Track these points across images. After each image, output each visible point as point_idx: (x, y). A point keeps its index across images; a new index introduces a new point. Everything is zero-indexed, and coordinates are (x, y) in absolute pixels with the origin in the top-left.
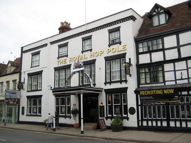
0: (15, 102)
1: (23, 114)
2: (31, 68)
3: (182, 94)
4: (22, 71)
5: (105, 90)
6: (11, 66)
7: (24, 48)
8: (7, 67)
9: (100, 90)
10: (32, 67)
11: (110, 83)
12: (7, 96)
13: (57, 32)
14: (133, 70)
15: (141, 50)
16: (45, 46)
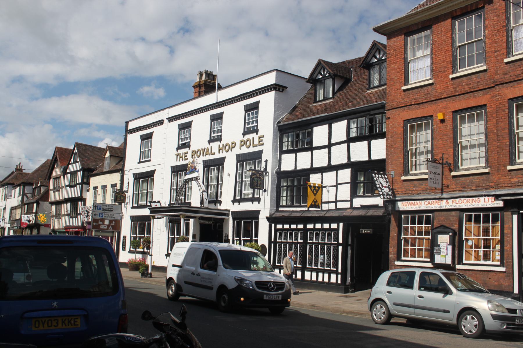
0: (111, 227)
1: (124, 249)
2: (138, 163)
3: (284, 228)
4: (126, 168)
5: (234, 213)
6: (111, 156)
7: (130, 123)
8: (105, 158)
9: (225, 213)
10: (140, 162)
11: (240, 201)
12: (95, 215)
13: (218, 82)
14: (268, 182)
15: (285, 148)
16: (161, 125)
